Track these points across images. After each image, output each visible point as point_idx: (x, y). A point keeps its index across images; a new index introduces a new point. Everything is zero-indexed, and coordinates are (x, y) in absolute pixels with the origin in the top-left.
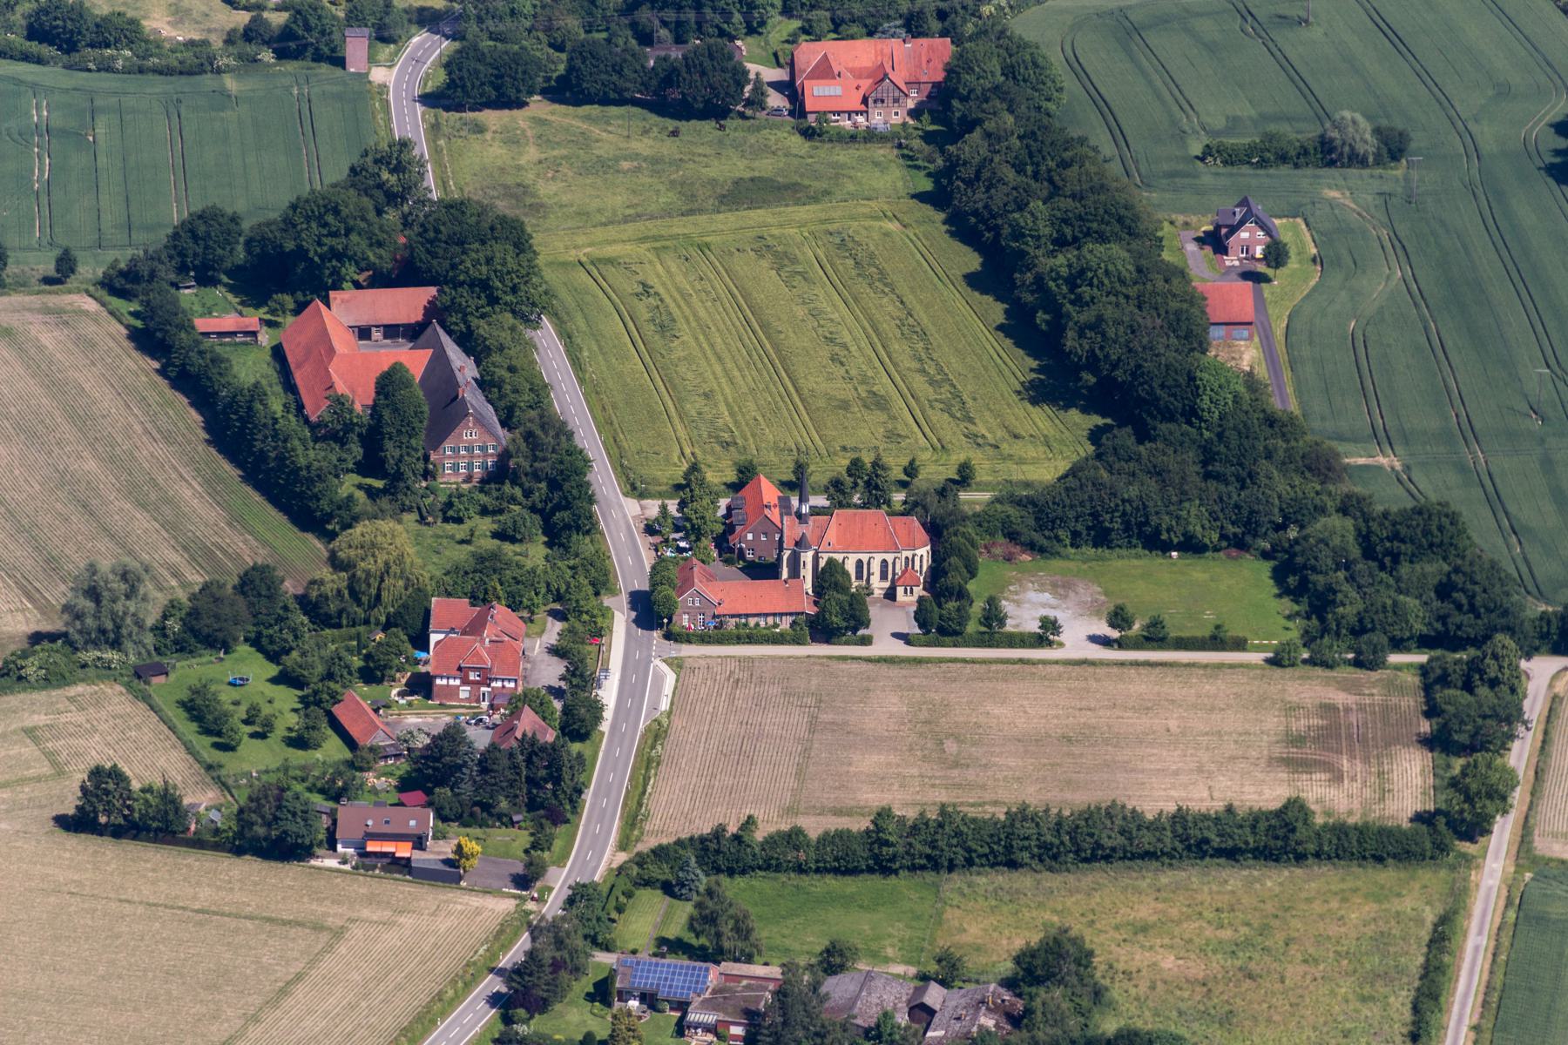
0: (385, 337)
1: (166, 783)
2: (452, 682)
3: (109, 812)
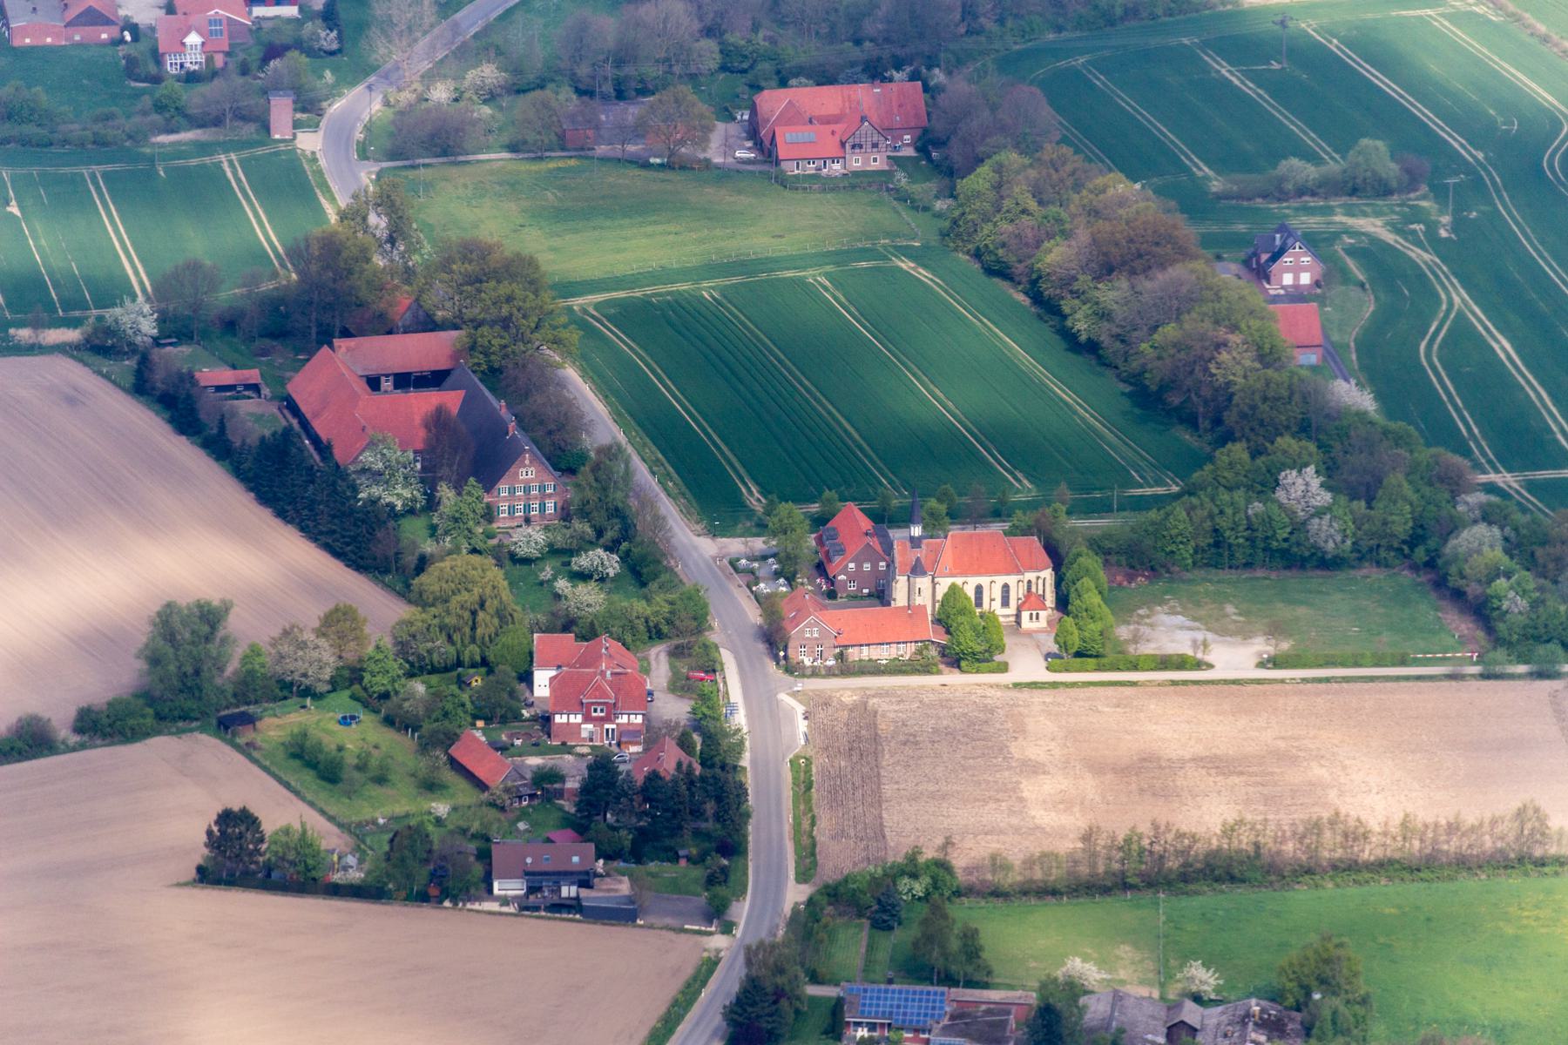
0: (396, 387)
1: (303, 824)
3: (236, 857)
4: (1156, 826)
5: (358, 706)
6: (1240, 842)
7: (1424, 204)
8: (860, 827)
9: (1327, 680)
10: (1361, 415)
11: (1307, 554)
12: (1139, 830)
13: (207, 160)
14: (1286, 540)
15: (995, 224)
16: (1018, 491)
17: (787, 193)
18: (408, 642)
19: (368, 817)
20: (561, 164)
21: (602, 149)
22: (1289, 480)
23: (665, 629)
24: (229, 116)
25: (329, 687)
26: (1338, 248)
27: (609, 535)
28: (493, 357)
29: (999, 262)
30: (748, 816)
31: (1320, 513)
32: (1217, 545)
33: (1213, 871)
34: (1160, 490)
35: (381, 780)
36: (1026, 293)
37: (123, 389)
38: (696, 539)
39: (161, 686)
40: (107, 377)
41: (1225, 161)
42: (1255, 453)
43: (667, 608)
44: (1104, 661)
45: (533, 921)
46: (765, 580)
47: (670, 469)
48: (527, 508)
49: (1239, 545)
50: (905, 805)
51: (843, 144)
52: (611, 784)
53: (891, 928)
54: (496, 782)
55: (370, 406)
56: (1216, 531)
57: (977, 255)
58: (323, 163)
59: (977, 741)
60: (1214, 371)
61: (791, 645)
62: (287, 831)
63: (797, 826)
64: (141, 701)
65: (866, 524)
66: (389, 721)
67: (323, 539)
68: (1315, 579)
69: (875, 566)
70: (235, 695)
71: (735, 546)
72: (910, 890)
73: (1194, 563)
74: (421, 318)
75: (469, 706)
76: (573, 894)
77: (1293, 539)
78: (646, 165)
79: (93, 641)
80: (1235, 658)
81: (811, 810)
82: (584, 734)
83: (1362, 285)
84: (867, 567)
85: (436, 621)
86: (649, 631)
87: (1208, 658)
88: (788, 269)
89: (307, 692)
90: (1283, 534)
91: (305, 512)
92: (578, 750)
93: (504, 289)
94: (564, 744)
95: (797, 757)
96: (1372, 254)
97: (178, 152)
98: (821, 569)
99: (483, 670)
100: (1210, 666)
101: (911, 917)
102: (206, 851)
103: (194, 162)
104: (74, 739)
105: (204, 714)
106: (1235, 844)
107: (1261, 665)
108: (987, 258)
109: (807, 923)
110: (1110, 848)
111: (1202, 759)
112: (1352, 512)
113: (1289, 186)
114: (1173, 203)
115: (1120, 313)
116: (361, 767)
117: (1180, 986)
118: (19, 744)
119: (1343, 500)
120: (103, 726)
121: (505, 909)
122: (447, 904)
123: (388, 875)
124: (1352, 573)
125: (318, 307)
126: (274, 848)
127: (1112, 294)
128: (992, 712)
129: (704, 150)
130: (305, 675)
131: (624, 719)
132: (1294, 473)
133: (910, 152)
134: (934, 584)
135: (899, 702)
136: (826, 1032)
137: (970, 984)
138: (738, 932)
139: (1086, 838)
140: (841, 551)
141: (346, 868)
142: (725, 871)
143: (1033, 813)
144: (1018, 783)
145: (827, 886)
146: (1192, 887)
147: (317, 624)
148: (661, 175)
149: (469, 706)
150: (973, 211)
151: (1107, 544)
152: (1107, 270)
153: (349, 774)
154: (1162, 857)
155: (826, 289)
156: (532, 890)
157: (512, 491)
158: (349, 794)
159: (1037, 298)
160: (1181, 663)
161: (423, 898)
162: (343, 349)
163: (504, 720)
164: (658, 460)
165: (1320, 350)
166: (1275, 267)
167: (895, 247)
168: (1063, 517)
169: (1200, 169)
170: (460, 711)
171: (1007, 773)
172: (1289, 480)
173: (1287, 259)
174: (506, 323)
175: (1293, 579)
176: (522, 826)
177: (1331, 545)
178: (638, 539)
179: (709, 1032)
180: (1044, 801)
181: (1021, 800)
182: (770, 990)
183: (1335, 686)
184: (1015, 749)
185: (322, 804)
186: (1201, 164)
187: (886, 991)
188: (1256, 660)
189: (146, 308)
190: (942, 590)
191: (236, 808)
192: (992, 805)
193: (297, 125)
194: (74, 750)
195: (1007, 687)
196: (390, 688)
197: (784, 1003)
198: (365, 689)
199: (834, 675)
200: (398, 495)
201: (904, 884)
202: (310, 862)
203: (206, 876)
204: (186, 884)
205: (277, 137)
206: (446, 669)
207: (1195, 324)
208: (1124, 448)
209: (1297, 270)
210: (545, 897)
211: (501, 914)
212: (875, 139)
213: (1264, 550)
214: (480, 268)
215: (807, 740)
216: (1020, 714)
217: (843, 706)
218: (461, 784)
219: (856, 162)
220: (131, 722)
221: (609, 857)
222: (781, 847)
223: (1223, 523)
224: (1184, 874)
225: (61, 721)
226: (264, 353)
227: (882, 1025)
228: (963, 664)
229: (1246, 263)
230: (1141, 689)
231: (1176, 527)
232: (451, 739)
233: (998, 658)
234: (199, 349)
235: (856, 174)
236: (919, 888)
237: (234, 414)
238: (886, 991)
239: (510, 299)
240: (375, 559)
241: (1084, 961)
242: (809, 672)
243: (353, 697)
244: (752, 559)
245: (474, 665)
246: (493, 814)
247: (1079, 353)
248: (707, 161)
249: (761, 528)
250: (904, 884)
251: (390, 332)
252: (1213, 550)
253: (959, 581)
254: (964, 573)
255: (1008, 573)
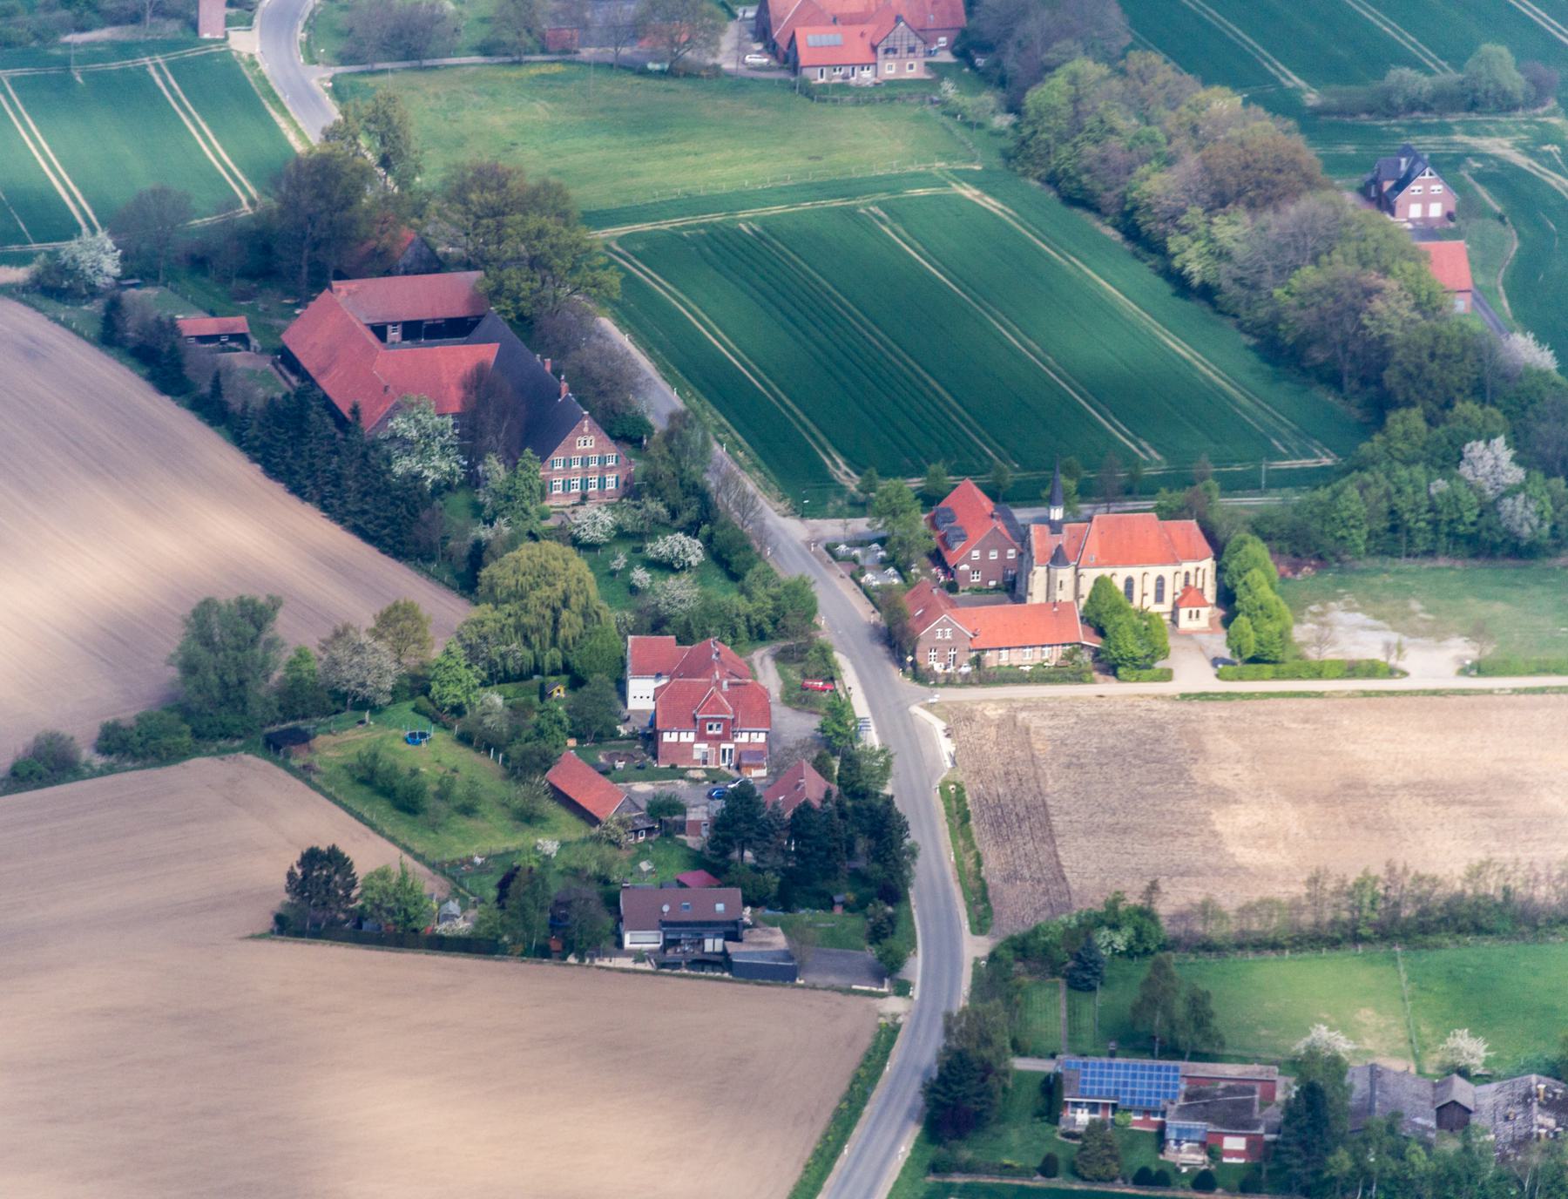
0: (405, 337)
2: (684, 738)
3: (320, 904)
4: (1391, 870)
5: (424, 721)
6: (1488, 885)
7: (1554, 121)
8: (1034, 866)
9: (1543, 690)
10: (1543, 374)
11: (1499, 540)
12: (1373, 873)
13: (129, 63)
14: (1473, 524)
15: (1075, 146)
16: (1146, 464)
17: (815, 106)
18: (478, 645)
19: (463, 855)
20: (544, 70)
21: (587, 53)
22: (1476, 453)
23: (769, 628)
24: (149, 12)
25: (388, 699)
26: (1464, 173)
27: (687, 516)
28: (522, 303)
29: (1081, 189)
30: (913, 853)
31: (1512, 492)
32: (1393, 529)
33: (1456, 920)
34: (1309, 463)
35: (467, 810)
36: (1116, 227)
37: (88, 340)
38: (781, 520)
39: (199, 698)
40: (65, 324)
41: (1316, 71)
42: (1431, 421)
43: (770, 604)
44: (1283, 667)
45: (673, 980)
46: (872, 569)
47: (738, 437)
48: (585, 483)
49: (1420, 530)
50: (1082, 841)
51: (874, 48)
52: (751, 818)
53: (1092, 989)
54: (609, 813)
55: (402, 359)
56: (1392, 512)
57: (1052, 180)
58: (264, 67)
59: (1157, 766)
60: (1366, 322)
61: (919, 648)
62: (383, 875)
63: (959, 865)
64: (176, 716)
65: (987, 504)
66: (465, 739)
67: (351, 520)
68: (1508, 569)
69: (1003, 554)
70: (281, 708)
71: (832, 528)
72: (1111, 943)
73: (1367, 550)
74: (424, 256)
75: (566, 722)
76: (719, 948)
77: (1483, 521)
78: (643, 72)
79: (112, 640)
80: (1433, 663)
81: (973, 846)
82: (697, 756)
83: (1501, 218)
84: (994, 555)
85: (511, 621)
86: (750, 632)
87: (1402, 665)
88: (834, 197)
89: (364, 705)
90: (1470, 516)
91: (328, 488)
92: (692, 774)
93: (534, 222)
94: (673, 767)
95: (945, 783)
96: (1502, 178)
97: (93, 54)
98: (937, 558)
99: (565, 678)
100: (1405, 674)
101: (1134, 976)
102: (287, 898)
103: (114, 66)
104: (99, 761)
105: (248, 730)
106: (1482, 891)
107: (1464, 672)
108: (1064, 184)
109: (994, 978)
110: (1336, 893)
111: (1415, 785)
112: (1549, 490)
113: (1399, 100)
114: (1291, 123)
115: (1240, 251)
116: (443, 795)
117: (1437, 1057)
118: (40, 767)
119: (1539, 476)
120: (129, 746)
121: (640, 966)
122: (572, 959)
123: (503, 925)
124: (1549, 562)
125: (303, 240)
126: (369, 894)
127: (1233, 229)
128: (1162, 728)
129: (714, 55)
130: (363, 685)
131: (744, 738)
132: (1482, 444)
133: (946, 57)
134: (1078, 577)
135: (1053, 717)
136: (1039, 1114)
137: (1198, 1056)
138: (915, 992)
139: (1313, 881)
140: (962, 537)
141: (450, 917)
142: (891, 919)
143: (1231, 850)
144: (1208, 814)
145: (1012, 939)
146: (1431, 939)
147: (372, 624)
148: (664, 84)
149: (566, 722)
150: (1048, 130)
151: (1268, 528)
152: (1219, 201)
153: (430, 803)
154: (1397, 904)
155: (882, 221)
156: (669, 944)
157: (568, 463)
158: (434, 827)
159: (1133, 233)
160: (1371, 670)
161: (543, 952)
162: (343, 293)
163: (599, 738)
164: (722, 425)
165: (1469, 295)
166: (1401, 198)
167: (953, 171)
168: (1215, 494)
169: (1288, 78)
170: (556, 728)
171: (1193, 803)
172: (1476, 453)
173: (1415, 188)
174: (535, 263)
175: (1483, 571)
176: (645, 866)
177: (1527, 530)
178: (721, 521)
179: (900, 1117)
180: (1242, 836)
181: (1215, 834)
182: (977, 1065)
183: (1553, 697)
184: (1196, 772)
185: (404, 840)
186: (1289, 73)
187: (1110, 1066)
188: (1458, 667)
189: (109, 244)
190: (1086, 588)
191: (323, 848)
192: (1182, 840)
193: (229, 22)
194: (101, 773)
195: (1173, 698)
196: (464, 700)
197: (991, 1079)
198: (432, 701)
199: (972, 684)
200: (438, 467)
201: (1103, 937)
202: (411, 910)
203: (286, 926)
204: (261, 937)
205: (207, 36)
206: (522, 677)
207: (1341, 266)
208: (1260, 413)
209: (1426, 200)
210: (690, 952)
211: (636, 972)
212: (912, 43)
213: (1448, 535)
214: (491, 200)
215: (954, 763)
216: (1195, 731)
217: (988, 722)
218: (563, 816)
219: (889, 69)
220: (166, 741)
221: (754, 905)
222: (947, 891)
223: (1402, 503)
224: (1422, 924)
225: (83, 736)
226: (246, 296)
227: (1106, 1106)
228: (1121, 671)
229: (1364, 191)
230: (1329, 702)
231: (1347, 508)
232: (546, 762)
233: (1159, 665)
234: (168, 292)
235: (891, 84)
236: (1120, 941)
237: (229, 371)
238: (1110, 1066)
239: (540, 234)
240: (417, 543)
241: (1331, 1029)
242: (942, 680)
243: (416, 710)
244: (853, 544)
245: (555, 672)
246: (608, 851)
247: (1187, 298)
248: (716, 67)
249: (859, 507)
250: (1103, 937)
251: (388, 273)
252: (1389, 535)
253: (1107, 572)
254: (1112, 563)
255: (1164, 562)
